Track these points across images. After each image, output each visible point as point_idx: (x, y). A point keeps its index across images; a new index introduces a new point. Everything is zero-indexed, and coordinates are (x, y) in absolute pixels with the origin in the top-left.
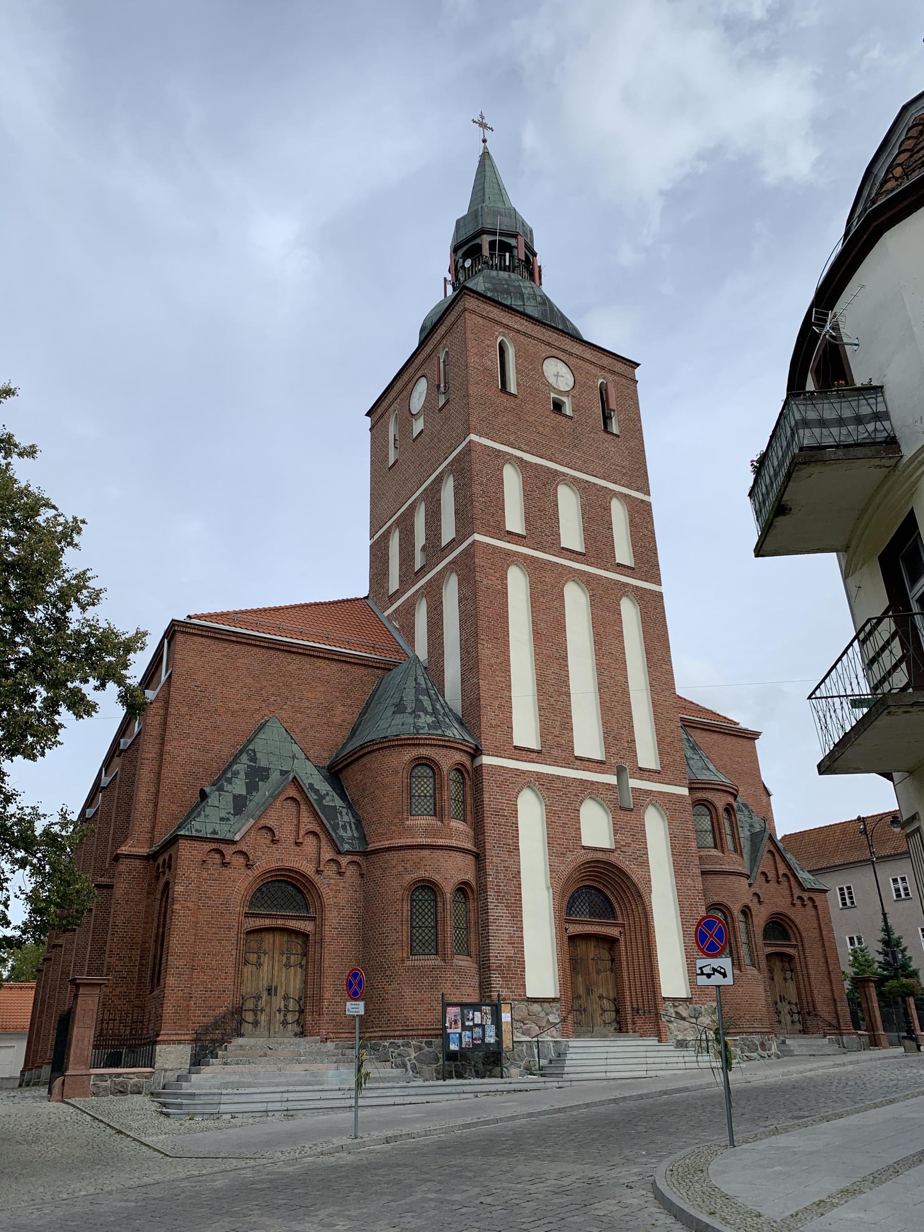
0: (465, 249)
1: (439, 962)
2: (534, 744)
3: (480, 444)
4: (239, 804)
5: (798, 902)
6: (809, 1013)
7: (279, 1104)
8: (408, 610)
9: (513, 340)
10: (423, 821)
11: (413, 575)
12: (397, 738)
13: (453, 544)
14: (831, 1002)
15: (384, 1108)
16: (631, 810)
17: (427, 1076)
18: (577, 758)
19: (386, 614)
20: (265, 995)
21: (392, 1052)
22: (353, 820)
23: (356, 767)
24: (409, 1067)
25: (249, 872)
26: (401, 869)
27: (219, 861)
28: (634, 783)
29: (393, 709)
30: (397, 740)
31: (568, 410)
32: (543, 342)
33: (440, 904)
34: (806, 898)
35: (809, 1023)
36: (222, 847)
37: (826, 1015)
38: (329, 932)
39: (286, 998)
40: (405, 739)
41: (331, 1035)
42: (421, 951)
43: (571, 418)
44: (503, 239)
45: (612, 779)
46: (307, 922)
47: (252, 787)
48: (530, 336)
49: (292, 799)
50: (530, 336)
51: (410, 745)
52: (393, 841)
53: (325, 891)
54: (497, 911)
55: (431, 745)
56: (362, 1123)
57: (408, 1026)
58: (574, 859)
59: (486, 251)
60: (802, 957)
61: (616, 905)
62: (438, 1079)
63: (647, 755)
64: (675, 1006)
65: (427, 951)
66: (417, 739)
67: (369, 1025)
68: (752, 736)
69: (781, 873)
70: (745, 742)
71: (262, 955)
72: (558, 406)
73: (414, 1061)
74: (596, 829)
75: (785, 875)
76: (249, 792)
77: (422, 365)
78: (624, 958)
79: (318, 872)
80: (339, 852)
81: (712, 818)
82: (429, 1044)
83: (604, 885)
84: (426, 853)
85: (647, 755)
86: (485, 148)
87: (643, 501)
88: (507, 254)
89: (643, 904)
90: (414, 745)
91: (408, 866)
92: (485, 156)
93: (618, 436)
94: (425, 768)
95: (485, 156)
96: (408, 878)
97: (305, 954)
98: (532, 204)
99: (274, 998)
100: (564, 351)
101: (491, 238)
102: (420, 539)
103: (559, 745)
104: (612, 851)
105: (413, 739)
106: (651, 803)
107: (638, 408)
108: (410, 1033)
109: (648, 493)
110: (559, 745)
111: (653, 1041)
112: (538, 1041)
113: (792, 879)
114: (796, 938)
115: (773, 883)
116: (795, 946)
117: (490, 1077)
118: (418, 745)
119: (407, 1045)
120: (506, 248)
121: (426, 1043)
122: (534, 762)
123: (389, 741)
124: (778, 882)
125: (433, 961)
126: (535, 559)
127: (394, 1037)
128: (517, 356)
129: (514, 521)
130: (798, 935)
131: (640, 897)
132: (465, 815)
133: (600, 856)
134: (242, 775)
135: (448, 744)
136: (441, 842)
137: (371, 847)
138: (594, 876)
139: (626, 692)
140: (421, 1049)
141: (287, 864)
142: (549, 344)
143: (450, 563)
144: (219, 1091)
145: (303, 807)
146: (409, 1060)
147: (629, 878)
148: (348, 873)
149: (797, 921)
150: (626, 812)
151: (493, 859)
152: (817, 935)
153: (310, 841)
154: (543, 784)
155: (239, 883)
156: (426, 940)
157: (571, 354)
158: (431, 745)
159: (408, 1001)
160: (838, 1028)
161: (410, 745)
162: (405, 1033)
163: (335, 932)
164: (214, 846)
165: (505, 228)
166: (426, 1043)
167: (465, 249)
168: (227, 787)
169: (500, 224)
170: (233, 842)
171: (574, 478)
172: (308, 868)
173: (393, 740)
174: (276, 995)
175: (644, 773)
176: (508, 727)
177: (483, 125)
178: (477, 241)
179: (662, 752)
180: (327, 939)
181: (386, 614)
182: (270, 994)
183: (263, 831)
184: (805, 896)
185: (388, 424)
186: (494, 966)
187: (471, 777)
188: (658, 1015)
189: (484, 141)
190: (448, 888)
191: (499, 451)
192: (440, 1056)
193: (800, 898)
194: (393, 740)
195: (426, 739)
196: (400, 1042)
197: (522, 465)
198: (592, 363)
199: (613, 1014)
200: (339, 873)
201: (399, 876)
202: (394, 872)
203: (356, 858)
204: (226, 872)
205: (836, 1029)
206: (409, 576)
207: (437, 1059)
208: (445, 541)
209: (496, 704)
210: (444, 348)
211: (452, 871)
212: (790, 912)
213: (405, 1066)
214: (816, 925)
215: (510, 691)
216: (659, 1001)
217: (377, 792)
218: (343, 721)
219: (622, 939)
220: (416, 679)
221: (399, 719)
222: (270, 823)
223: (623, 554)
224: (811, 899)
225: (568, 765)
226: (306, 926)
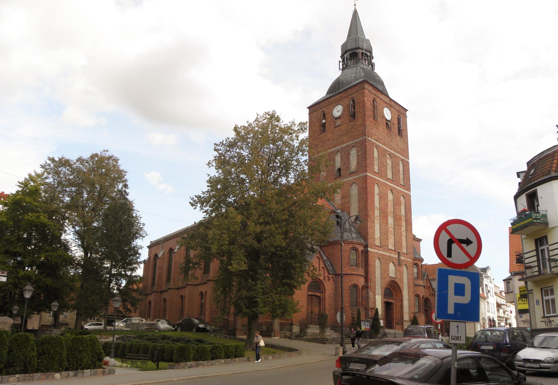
38: (327, 297)
53: (326, 285)
58: (388, 280)
68: (419, 240)
75: (323, 268)
79: (324, 279)
86: (355, 8)
89: (401, 294)
92: (355, 13)
95: (355, 13)
96: (350, 283)
101: (362, 51)
109: (408, 159)
133: (393, 279)
150: (399, 263)
167: (351, 52)
169: (365, 46)
187: (366, 253)
189: (355, 5)
190: (360, 287)
201: (348, 282)
208: (339, 154)
211: (361, 282)
212: (429, 297)
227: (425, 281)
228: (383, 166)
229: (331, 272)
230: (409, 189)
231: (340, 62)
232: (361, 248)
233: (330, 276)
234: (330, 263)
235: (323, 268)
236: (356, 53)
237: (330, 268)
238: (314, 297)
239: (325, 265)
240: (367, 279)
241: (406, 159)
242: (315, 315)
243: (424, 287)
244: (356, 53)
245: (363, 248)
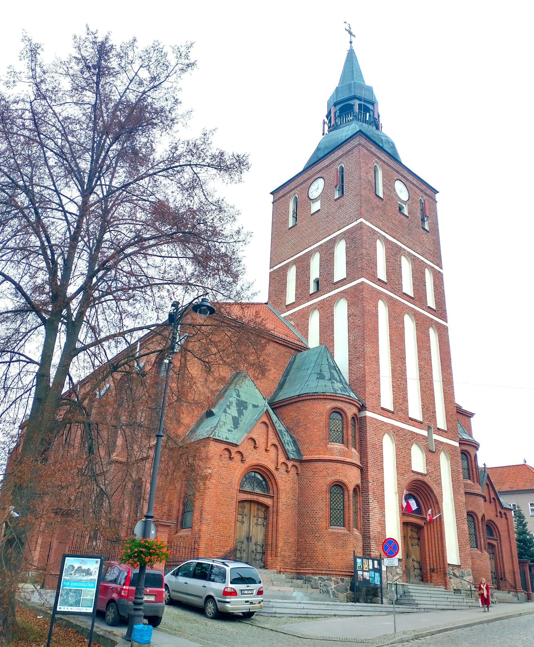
0: (341, 105)
1: (346, 531)
2: (391, 408)
3: (366, 225)
4: (236, 422)
5: (499, 514)
6: (501, 579)
7: (299, 610)
8: (304, 316)
9: (382, 167)
10: (338, 446)
11: (308, 296)
12: (324, 394)
13: (342, 282)
14: (512, 573)
15: (349, 618)
16: (434, 452)
17: (342, 599)
18: (410, 419)
19: (283, 315)
20: (245, 541)
21: (320, 583)
22: (291, 440)
23: (290, 408)
24: (331, 593)
25: (242, 464)
26: (325, 473)
27: (228, 456)
28: (435, 437)
29: (316, 376)
30: (324, 395)
31: (406, 212)
32: (395, 170)
33: (346, 497)
34: (503, 513)
35: (501, 584)
36: (230, 447)
37: (509, 580)
38: (282, 507)
39: (256, 544)
40: (328, 395)
41: (282, 570)
42: (335, 523)
43: (406, 216)
44: (365, 104)
45: (425, 433)
46: (269, 499)
47: (240, 413)
48: (389, 166)
49: (264, 423)
50: (389, 166)
51: (330, 399)
52: (313, 456)
53: (279, 481)
54: (373, 505)
55: (342, 401)
56: (91, 607)
57: (329, 568)
58: (409, 478)
59: (356, 109)
60: (499, 546)
61: (423, 507)
62: (347, 602)
63: (441, 423)
64: (453, 569)
65: (338, 524)
66: (336, 396)
67: (302, 565)
69: (492, 497)
70: (466, 418)
71: (244, 516)
72: (400, 209)
73: (334, 590)
74: (418, 462)
75: (493, 498)
76: (239, 416)
77: (320, 171)
78: (426, 538)
79: (277, 469)
80: (288, 458)
81: (468, 462)
82: (342, 580)
83: (418, 494)
84: (340, 465)
85: (441, 423)
87: (439, 272)
88: (368, 114)
89: (439, 508)
90: (333, 399)
91: (329, 472)
92: (351, 57)
93: (428, 232)
94: (338, 414)
95: (351, 57)
96: (330, 479)
97: (266, 518)
98: (110, 37)
99: (250, 543)
100: (404, 177)
102: (315, 273)
103: (402, 410)
104: (426, 475)
105: (333, 396)
106: (442, 449)
107: (437, 217)
108: (331, 572)
109: (441, 268)
110: (402, 410)
111: (442, 588)
112: (396, 584)
113: (497, 501)
114: (497, 535)
115: (488, 502)
116: (496, 540)
117: (370, 603)
118: (335, 400)
119: (330, 580)
120: (367, 110)
121: (341, 579)
122: (390, 418)
123: (318, 395)
124: (490, 502)
125: (342, 530)
126: (391, 298)
127: (322, 574)
128: (383, 177)
129: (382, 274)
130: (498, 534)
131: (437, 503)
132: (355, 445)
133: (420, 477)
134: (234, 404)
135: (351, 402)
136: (348, 460)
137: (305, 458)
138: (414, 489)
139: (431, 383)
140: (338, 583)
141: (262, 463)
142: (398, 172)
143: (340, 292)
144: (269, 600)
145: (270, 429)
146: (331, 589)
147: (432, 492)
148: (291, 473)
149: (498, 526)
150: (431, 453)
151: (372, 473)
152: (507, 534)
153: (272, 450)
154: (396, 432)
155: (238, 470)
156: (338, 517)
157: (408, 180)
158: (342, 401)
159: (329, 553)
160: (515, 588)
161: (330, 399)
162: (328, 572)
163: (284, 507)
164: (226, 446)
165: (366, 97)
166: (341, 579)
167: (341, 105)
168: (228, 411)
169: (363, 94)
170: (236, 445)
171: (409, 253)
172: (272, 467)
173: (321, 395)
174: (251, 541)
175: (439, 431)
176: (377, 396)
177: (351, 33)
178: (351, 102)
179: (448, 421)
180: (280, 511)
181: (283, 315)
182: (248, 541)
183: (250, 441)
184: (503, 511)
185: (289, 202)
186: (372, 537)
187: (360, 423)
188: (445, 574)
189: (351, 42)
190: (351, 488)
191: (375, 231)
192: (348, 588)
193: (500, 512)
194: (321, 395)
195: (340, 397)
196: (325, 577)
197: (386, 241)
198: (417, 187)
199: (419, 571)
200: (287, 471)
202: (321, 474)
203: (297, 464)
204: (232, 463)
205: (514, 588)
206: (302, 294)
207: (347, 590)
208: (336, 279)
209: (373, 381)
210: (340, 164)
211: (352, 478)
213: (328, 592)
214: (506, 529)
215: (379, 374)
216: (446, 566)
217: (309, 425)
218: (274, 378)
219: (425, 527)
220: (328, 360)
221: (322, 382)
222: (254, 437)
223: (431, 302)
224: (505, 513)
225: (406, 422)
226: (268, 501)
227: (485, 486)
228: (394, 270)
229: (291, 456)
230: (444, 317)
231: (324, 123)
232: (351, 411)
233: (290, 464)
234: (291, 437)
235: (274, 445)
236: (352, 106)
237: (290, 448)
238: (254, 507)
239: (280, 440)
240: (363, 470)
241: (440, 270)
242: (256, 544)
243: (484, 497)
244: (352, 106)
245: (355, 410)
